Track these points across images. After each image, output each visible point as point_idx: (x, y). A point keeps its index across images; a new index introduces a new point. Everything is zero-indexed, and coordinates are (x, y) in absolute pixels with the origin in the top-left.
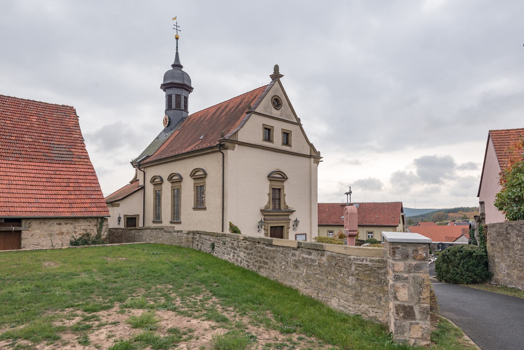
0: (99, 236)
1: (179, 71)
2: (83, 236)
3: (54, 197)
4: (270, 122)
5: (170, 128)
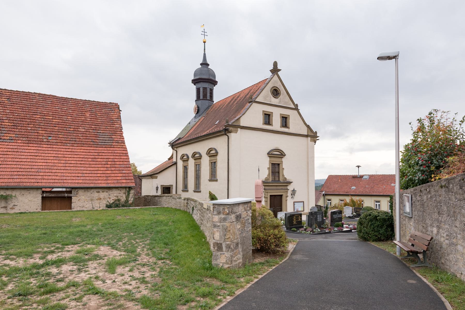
0: (127, 201)
1: (205, 69)
2: (115, 201)
3: (95, 172)
4: (269, 109)
5: (198, 114)
